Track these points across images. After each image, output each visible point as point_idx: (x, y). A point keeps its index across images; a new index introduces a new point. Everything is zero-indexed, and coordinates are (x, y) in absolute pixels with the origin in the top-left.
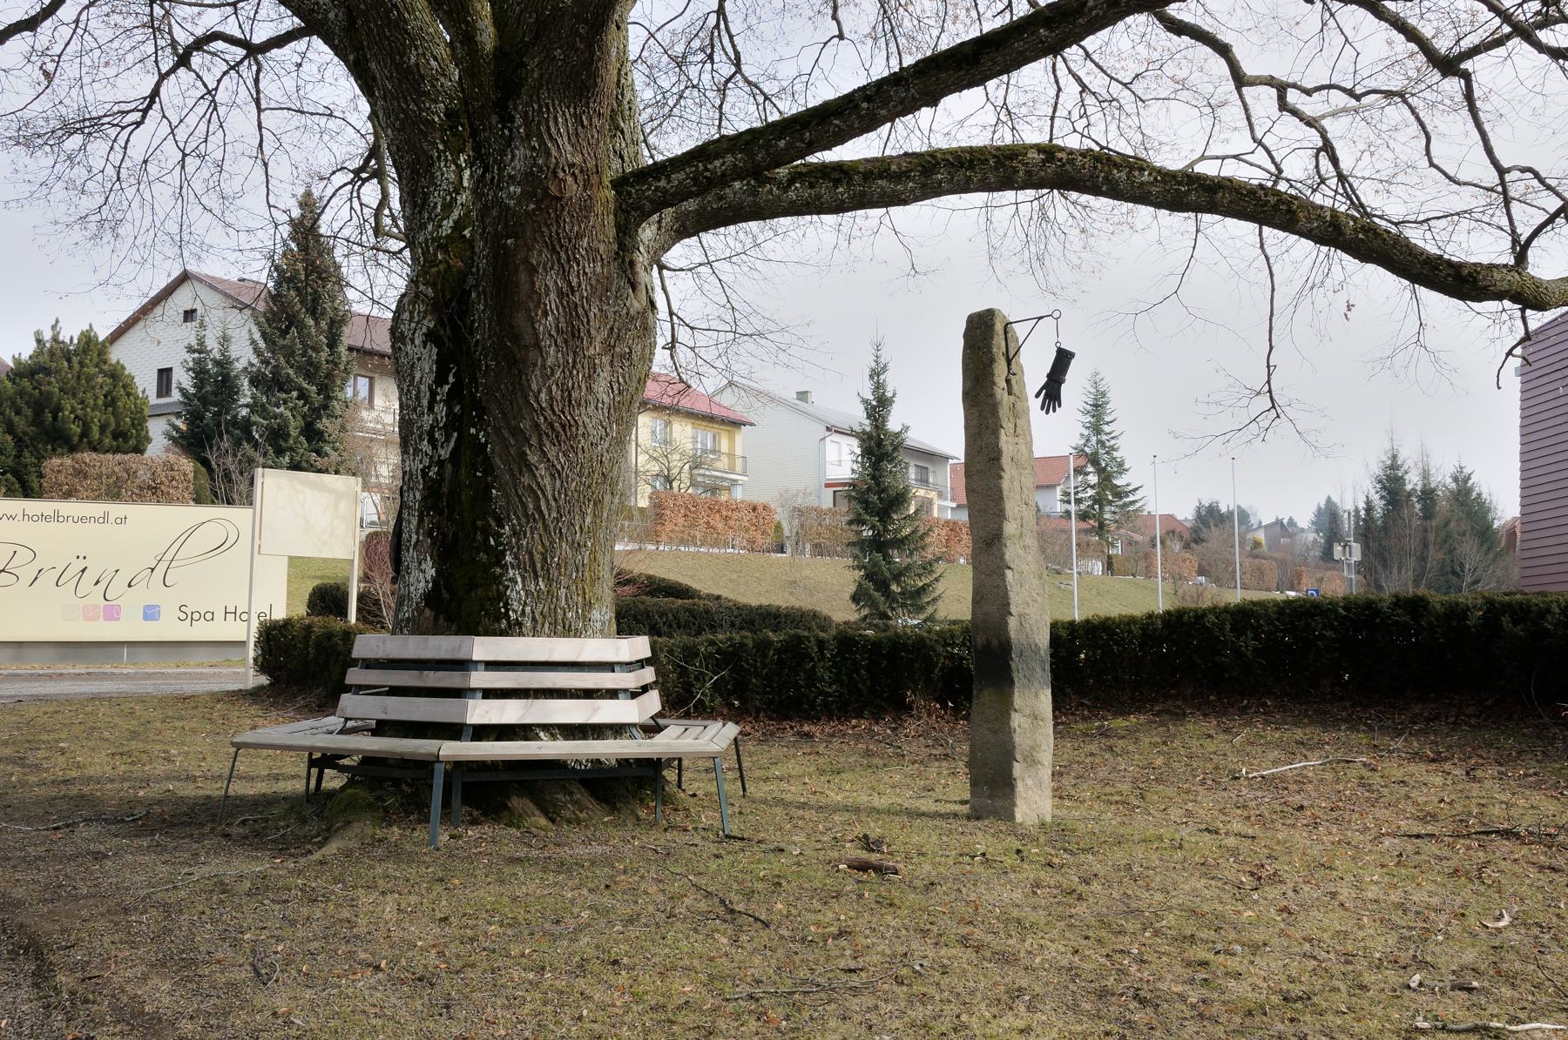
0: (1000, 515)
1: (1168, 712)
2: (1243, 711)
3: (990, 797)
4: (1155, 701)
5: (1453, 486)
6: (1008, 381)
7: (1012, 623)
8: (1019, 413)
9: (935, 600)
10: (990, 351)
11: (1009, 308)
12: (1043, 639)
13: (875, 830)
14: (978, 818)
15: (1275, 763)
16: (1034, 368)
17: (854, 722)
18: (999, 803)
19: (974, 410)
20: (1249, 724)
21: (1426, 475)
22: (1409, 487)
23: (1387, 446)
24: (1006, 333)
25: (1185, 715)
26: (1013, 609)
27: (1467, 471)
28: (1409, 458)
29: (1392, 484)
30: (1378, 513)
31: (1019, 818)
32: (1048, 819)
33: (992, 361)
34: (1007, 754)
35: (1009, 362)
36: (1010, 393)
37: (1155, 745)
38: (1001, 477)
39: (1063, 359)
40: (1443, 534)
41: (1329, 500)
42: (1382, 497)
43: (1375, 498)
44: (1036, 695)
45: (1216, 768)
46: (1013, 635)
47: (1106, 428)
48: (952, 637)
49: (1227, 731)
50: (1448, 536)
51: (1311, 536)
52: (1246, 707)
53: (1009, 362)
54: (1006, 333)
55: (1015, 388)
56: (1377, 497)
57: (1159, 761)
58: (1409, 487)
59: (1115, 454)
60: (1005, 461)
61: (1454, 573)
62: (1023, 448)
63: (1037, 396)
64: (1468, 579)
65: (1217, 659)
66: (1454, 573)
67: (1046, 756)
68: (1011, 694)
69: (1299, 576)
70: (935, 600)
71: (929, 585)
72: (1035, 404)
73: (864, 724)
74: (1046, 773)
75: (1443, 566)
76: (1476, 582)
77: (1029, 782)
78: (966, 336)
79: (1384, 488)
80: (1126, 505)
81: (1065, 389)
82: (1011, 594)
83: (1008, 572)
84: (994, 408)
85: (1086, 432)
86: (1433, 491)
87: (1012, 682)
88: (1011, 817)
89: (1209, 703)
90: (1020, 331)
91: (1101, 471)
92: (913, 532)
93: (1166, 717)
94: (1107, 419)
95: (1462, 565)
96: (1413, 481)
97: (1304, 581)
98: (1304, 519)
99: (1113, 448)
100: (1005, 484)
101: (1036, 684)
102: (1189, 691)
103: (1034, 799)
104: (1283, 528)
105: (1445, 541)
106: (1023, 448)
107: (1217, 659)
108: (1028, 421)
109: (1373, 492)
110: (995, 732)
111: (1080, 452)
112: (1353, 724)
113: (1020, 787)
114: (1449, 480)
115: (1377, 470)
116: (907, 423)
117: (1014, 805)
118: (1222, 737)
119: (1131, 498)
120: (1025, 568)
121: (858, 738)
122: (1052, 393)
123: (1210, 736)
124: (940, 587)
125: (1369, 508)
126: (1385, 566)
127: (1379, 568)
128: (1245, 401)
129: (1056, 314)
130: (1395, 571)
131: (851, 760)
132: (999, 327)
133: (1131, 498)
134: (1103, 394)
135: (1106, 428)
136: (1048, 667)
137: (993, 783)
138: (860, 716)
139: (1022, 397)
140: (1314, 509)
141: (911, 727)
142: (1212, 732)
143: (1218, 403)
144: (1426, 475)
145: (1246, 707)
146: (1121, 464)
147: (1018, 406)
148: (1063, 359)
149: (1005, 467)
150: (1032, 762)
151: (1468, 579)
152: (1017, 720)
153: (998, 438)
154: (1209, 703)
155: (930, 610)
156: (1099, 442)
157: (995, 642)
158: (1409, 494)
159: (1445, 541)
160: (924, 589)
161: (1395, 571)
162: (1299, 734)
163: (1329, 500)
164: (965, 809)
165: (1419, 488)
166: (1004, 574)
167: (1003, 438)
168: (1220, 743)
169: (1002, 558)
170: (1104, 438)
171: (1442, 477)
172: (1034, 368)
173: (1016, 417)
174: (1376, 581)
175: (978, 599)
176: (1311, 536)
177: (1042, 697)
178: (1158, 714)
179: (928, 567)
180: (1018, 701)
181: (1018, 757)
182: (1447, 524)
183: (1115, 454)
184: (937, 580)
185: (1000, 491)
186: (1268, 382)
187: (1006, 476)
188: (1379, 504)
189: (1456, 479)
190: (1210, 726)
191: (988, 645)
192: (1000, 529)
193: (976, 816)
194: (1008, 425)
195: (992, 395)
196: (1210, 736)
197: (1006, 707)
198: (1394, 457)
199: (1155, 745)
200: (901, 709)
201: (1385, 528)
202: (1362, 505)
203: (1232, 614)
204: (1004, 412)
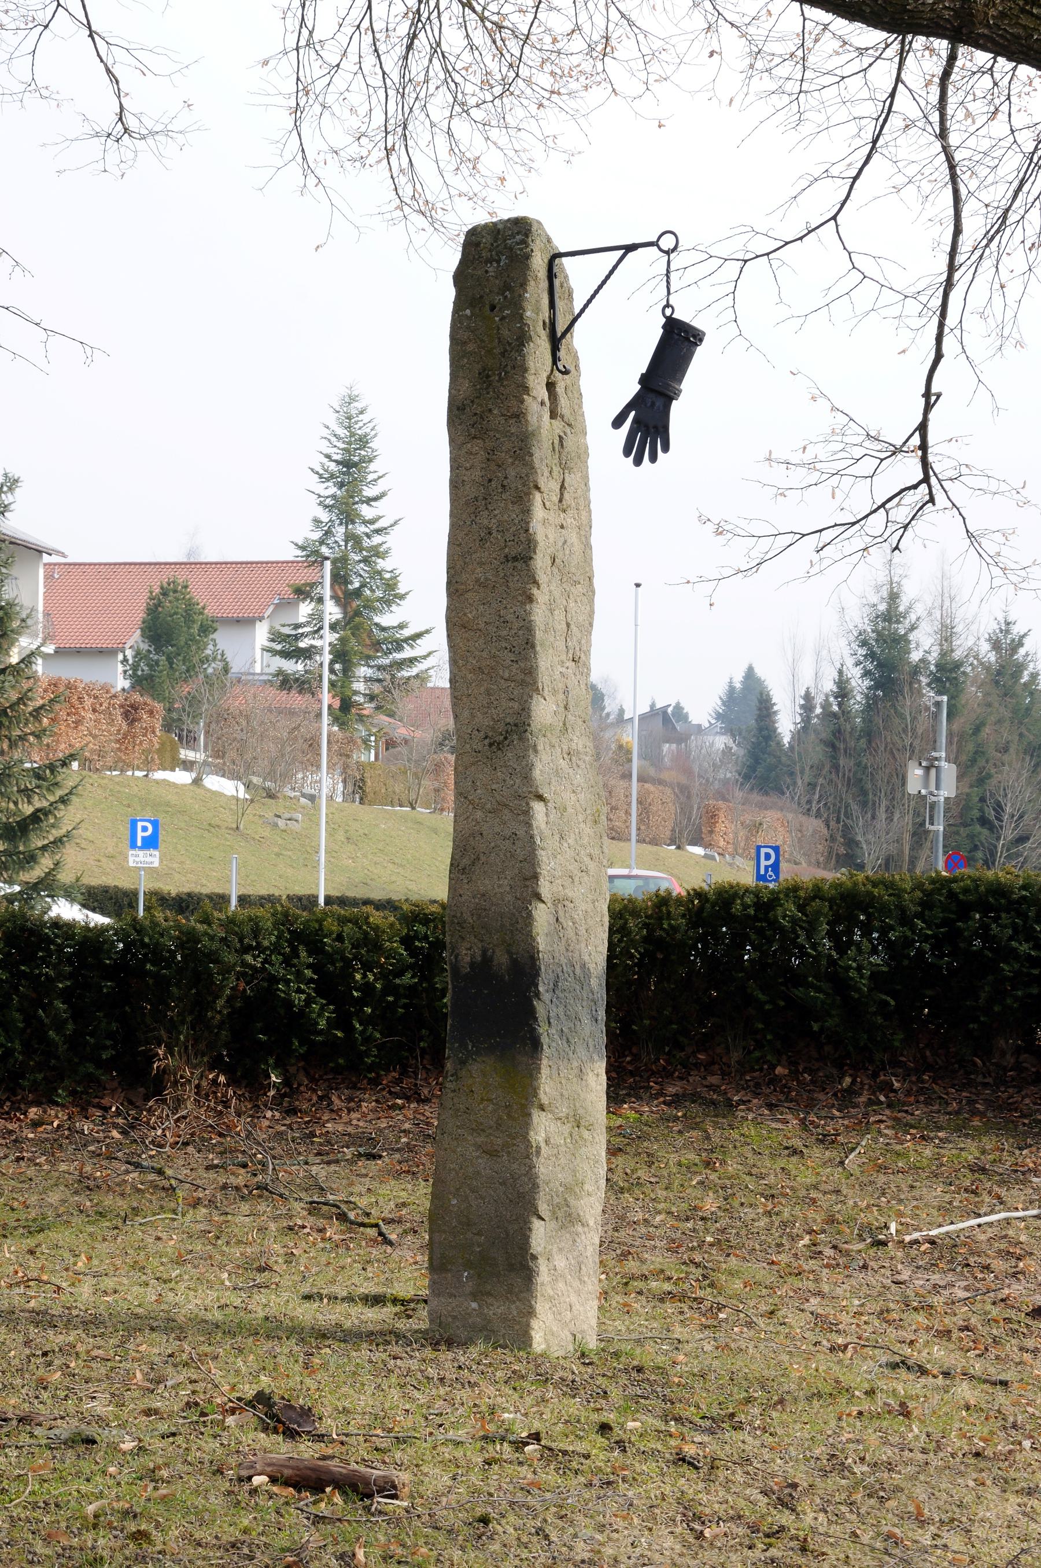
0: (527, 681)
1: (695, 1097)
2: (846, 1099)
3: (474, 1296)
4: (667, 1074)
5: (992, 657)
6: (550, 386)
7: (542, 915)
8: (570, 457)
9: (58, 842)
10: (518, 315)
11: (563, 224)
12: (594, 951)
13: (287, 1378)
14: (450, 1343)
15: (946, 1211)
16: (608, 361)
17: (33, 1112)
18: (496, 1309)
19: (476, 446)
20: (862, 1127)
21: (947, 634)
22: (915, 656)
23: (882, 578)
24: (551, 275)
25: (730, 1106)
26: (545, 888)
27: (1017, 630)
28: (918, 595)
29: (884, 649)
30: (857, 701)
31: (539, 1342)
32: (592, 1343)
33: (522, 338)
34: (517, 1201)
35: (555, 342)
36: (553, 415)
37: (690, 1168)
38: (530, 599)
39: (678, 342)
40: (970, 747)
41: (750, 674)
42: (866, 673)
43: (854, 674)
44: (581, 1074)
45: (831, 1220)
46: (542, 943)
47: (367, 511)
48: (256, 932)
49: (826, 1140)
50: (979, 752)
51: (721, 742)
52: (851, 1092)
53: (555, 342)
54: (551, 275)
55: (563, 401)
56: (857, 672)
57: (710, 1204)
58: (915, 656)
59: (381, 564)
60: (541, 562)
61: (984, 821)
62: (573, 538)
63: (617, 423)
64: (1008, 833)
65: (799, 992)
66: (984, 821)
67: (592, 1204)
68: (532, 1073)
69: (712, 817)
70: (58, 842)
71: (46, 812)
72: (604, 442)
73: (57, 1117)
74: (590, 1239)
75: (967, 808)
76: (1022, 839)
77: (560, 1262)
78: (460, 277)
79: (871, 655)
80: (400, 664)
81: (681, 414)
82: (543, 855)
83: (538, 807)
84: (522, 447)
85: (324, 516)
86: (958, 665)
87: (535, 1045)
88: (523, 1340)
89: (774, 1081)
90: (581, 276)
91: (346, 597)
92: (21, 700)
93: (695, 1108)
94: (369, 492)
95: (999, 808)
96: (924, 645)
97: (720, 827)
98: (702, 708)
99: (378, 552)
100: (539, 614)
101: (581, 1051)
102: (736, 1056)
103: (568, 1303)
104: (666, 722)
105: (973, 761)
106: (573, 538)
107: (799, 992)
108: (586, 479)
109: (850, 662)
110: (492, 1154)
111: (313, 556)
112: (777, 1096)
113: (543, 1274)
114: (985, 647)
115: (859, 619)
116: (14, 472)
117: (531, 1313)
118: (817, 1153)
119: (407, 653)
120: (569, 799)
121: (52, 1147)
122: (648, 421)
123: (795, 1152)
124: (68, 817)
125: (843, 692)
126: (864, 804)
127: (855, 807)
128: (868, 466)
129: (667, 243)
130: (882, 815)
131: (54, 1198)
132: (538, 263)
133: (407, 653)
134: (363, 441)
135: (367, 511)
136: (602, 1015)
137: (483, 1261)
138: (46, 1099)
139: (574, 424)
140: (720, 690)
141: (163, 1125)
142: (797, 1143)
143: (811, 466)
144: (947, 634)
145: (851, 1092)
146: (391, 585)
147: (569, 443)
148: (678, 342)
149: (542, 578)
150: (569, 1219)
151: (1008, 833)
152: (543, 1128)
153: (527, 512)
154: (774, 1081)
155: (46, 862)
156: (349, 537)
157: (501, 958)
158: (915, 671)
159: (973, 761)
160: (36, 817)
161: (882, 815)
162: (971, 1150)
163: (750, 674)
164: (421, 1320)
165: (933, 657)
166: (527, 812)
167: (538, 513)
168: (813, 1168)
169: (527, 777)
170: (361, 529)
171: (974, 642)
172: (608, 361)
173: (564, 467)
174: (847, 831)
175: (463, 865)
176: (721, 742)
177: (591, 1079)
178: (676, 1101)
179: (46, 775)
180: (547, 1087)
181: (543, 1208)
182: (977, 730)
183: (381, 564)
184: (63, 801)
185: (528, 628)
186: (922, 428)
187: (541, 596)
188: (859, 685)
189: (996, 645)
190: (787, 1128)
191: (484, 966)
192: (525, 711)
193: (442, 1337)
194: (549, 485)
195: (519, 416)
196: (795, 1152)
197: (522, 1099)
198: (893, 597)
199: (690, 1168)
200: (143, 1084)
201: (869, 734)
202: (829, 685)
203: (831, 901)
204: (542, 455)
